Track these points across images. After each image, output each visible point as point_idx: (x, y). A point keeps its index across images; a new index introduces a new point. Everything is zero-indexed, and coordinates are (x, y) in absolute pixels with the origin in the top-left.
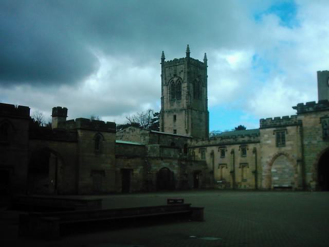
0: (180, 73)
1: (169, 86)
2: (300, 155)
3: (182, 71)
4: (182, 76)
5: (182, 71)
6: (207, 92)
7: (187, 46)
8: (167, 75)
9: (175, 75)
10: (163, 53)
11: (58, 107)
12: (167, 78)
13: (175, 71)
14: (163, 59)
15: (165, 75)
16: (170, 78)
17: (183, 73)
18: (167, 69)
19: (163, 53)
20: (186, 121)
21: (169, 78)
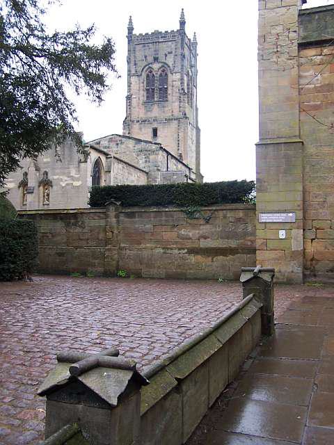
0: (166, 55)
4: (170, 61)
5: (171, 53)
9: (156, 59)
14: (130, 29)
16: (145, 63)
17: (172, 55)
18: (138, 48)
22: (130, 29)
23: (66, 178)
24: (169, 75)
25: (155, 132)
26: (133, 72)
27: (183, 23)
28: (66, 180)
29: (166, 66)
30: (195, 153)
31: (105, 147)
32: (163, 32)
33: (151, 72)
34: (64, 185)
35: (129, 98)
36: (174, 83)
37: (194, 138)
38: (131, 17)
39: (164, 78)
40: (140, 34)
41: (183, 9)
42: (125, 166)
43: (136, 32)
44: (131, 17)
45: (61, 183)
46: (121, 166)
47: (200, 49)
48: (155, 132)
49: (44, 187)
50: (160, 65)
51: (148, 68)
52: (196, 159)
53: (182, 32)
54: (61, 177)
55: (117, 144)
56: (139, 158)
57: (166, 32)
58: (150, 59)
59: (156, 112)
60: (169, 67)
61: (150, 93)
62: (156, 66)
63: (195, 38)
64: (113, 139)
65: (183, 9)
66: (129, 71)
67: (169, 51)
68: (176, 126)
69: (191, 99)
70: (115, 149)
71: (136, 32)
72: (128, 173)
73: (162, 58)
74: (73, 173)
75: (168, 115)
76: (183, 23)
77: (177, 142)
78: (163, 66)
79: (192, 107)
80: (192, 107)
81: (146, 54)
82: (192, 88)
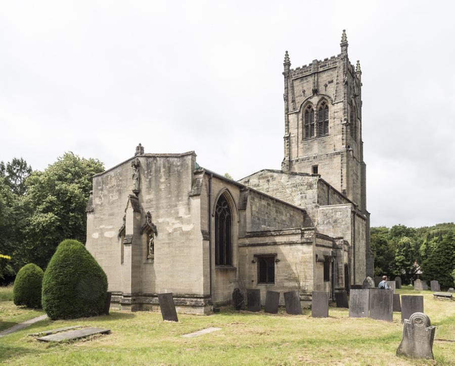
0: (326, 86)
1: (300, 115)
2: (322, 263)
3: (331, 82)
4: (331, 91)
5: (332, 82)
6: (361, 111)
7: (285, 53)
8: (297, 94)
9: (315, 92)
10: (287, 55)
11: (361, 102)
12: (297, 100)
13: (316, 84)
14: (287, 64)
15: (293, 94)
16: (303, 99)
17: (333, 85)
18: (296, 83)
19: (287, 55)
20: (118, 293)
21: (300, 100)
22: (287, 64)
23: (174, 221)
24: (330, 105)
25: (315, 169)
26: (291, 109)
27: (344, 45)
28: (173, 224)
29: (326, 97)
30: (360, 189)
31: (255, 186)
32: (323, 60)
33: (310, 107)
34: (170, 231)
35: (288, 138)
36: (336, 114)
37: (359, 174)
38: (287, 52)
39: (324, 108)
40: (297, 69)
41: (344, 31)
42: (270, 202)
43: (293, 67)
44: (287, 52)
45: (168, 228)
46: (264, 203)
47: (363, 80)
48: (315, 169)
49: (148, 234)
50: (320, 97)
51: (306, 104)
52: (361, 196)
53: (344, 57)
54: (168, 220)
55: (268, 181)
56: (293, 194)
57: (326, 60)
58: (309, 93)
59: (316, 148)
60: (330, 98)
61: (308, 133)
62: (315, 100)
63: (358, 64)
64: (266, 174)
65: (344, 31)
66: (287, 109)
67: (330, 80)
68: (340, 161)
69: (355, 133)
70: (266, 186)
71: (293, 67)
72: (277, 212)
73: (322, 90)
74: (182, 211)
75: (331, 151)
76: (344, 45)
77: (340, 178)
78: (323, 98)
79: (356, 141)
80: (356, 141)
81: (305, 88)
82: (356, 121)
